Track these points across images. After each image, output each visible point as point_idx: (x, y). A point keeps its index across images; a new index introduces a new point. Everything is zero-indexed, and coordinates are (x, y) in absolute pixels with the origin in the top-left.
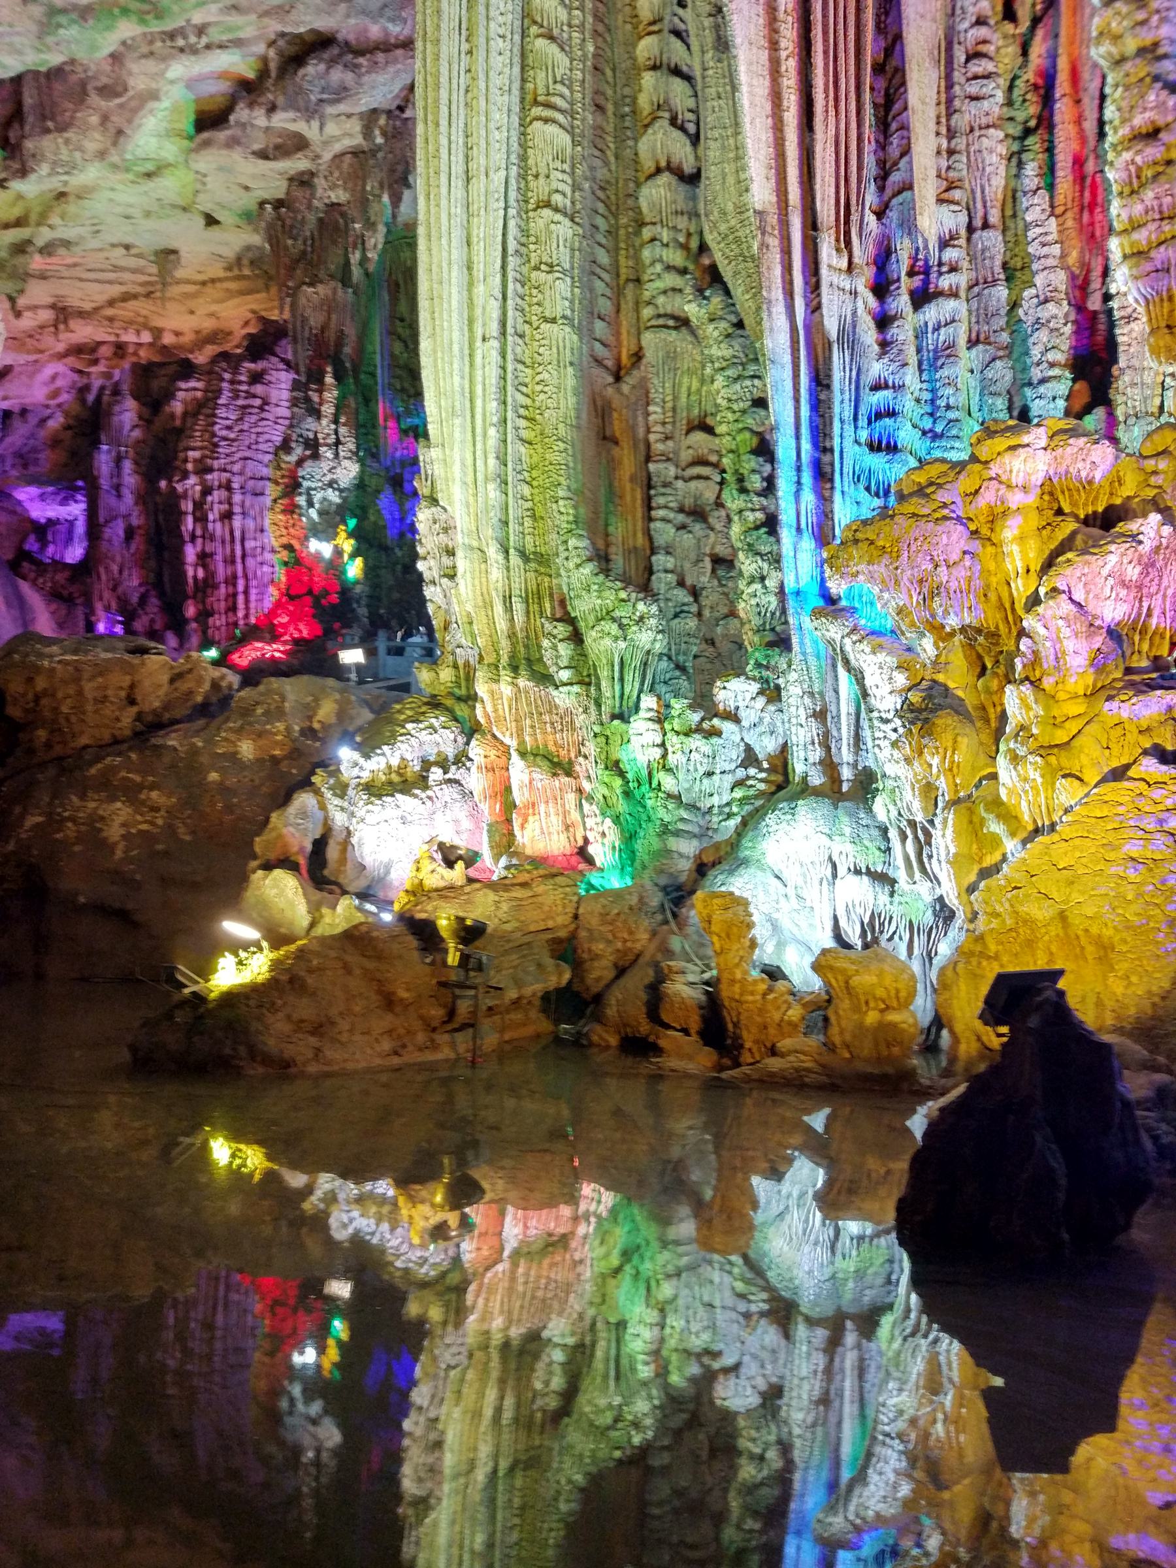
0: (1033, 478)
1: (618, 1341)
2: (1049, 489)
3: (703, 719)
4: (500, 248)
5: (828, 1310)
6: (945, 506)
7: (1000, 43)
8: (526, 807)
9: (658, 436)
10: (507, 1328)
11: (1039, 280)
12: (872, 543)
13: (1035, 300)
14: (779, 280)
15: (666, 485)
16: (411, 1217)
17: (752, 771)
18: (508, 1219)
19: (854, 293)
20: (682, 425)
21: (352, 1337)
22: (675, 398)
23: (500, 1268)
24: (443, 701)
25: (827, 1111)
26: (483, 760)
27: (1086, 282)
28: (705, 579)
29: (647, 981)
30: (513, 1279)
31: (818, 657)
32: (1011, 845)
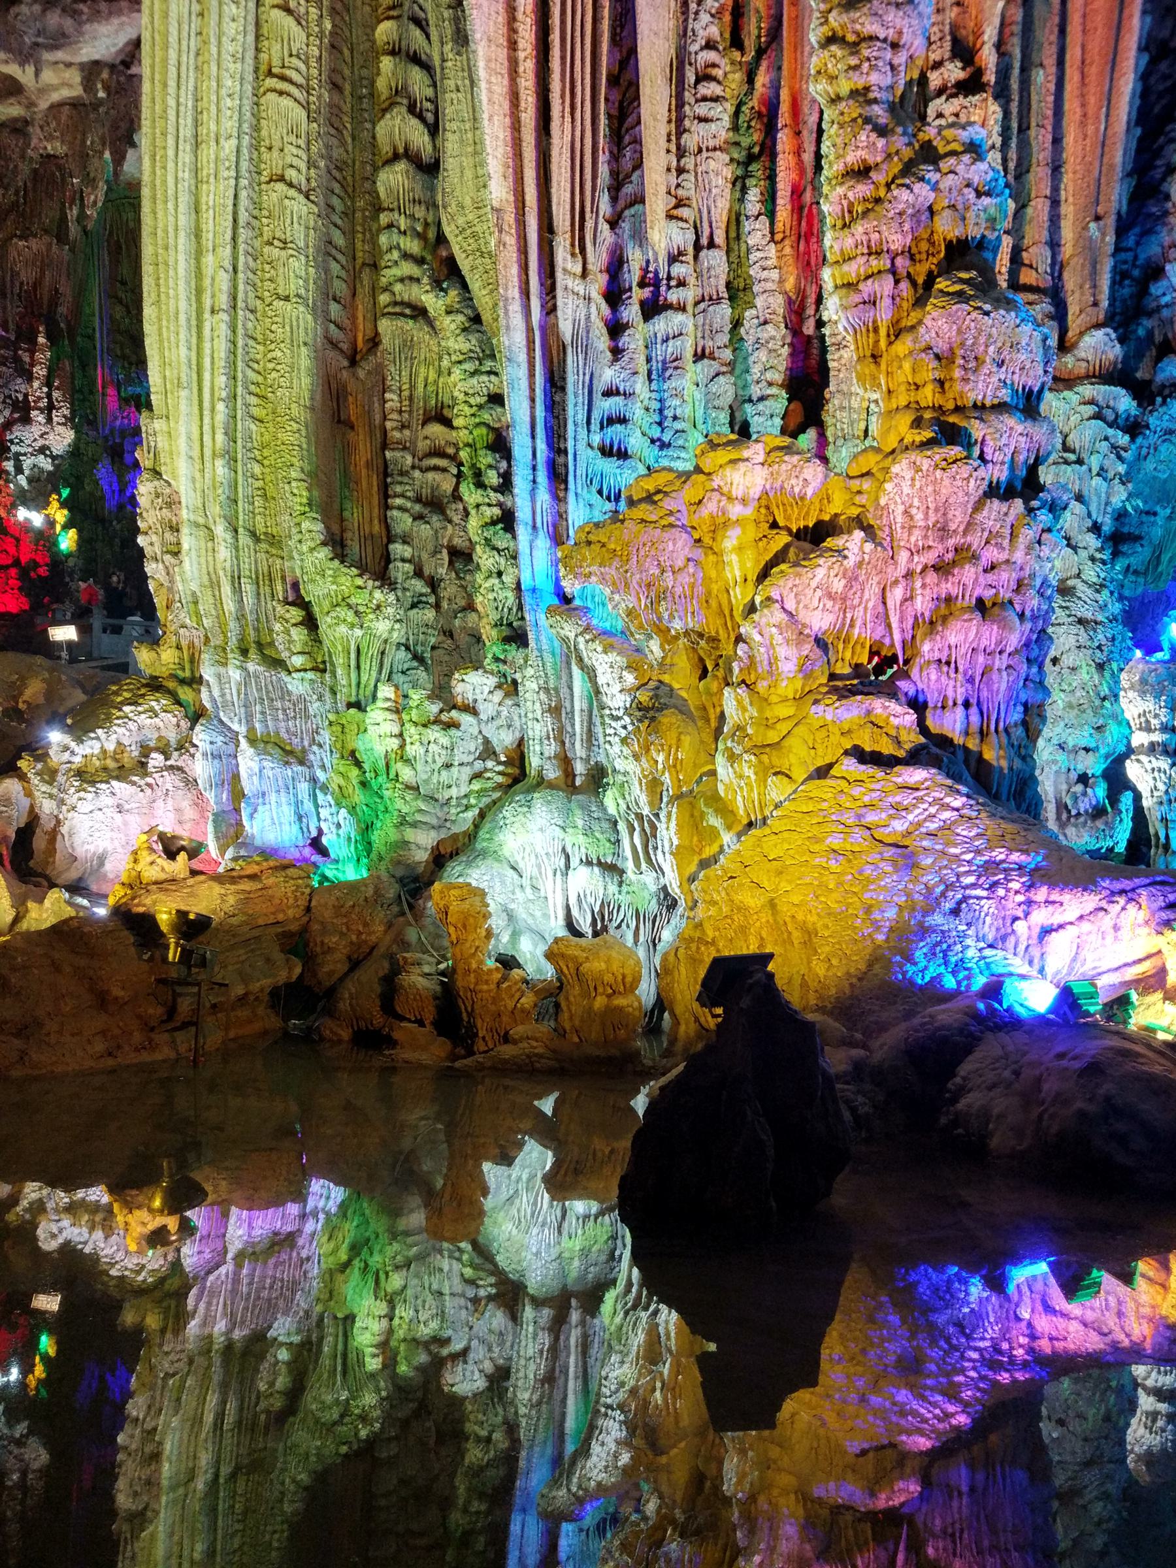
0: (751, 492)
1: (346, 1336)
2: (765, 502)
3: (441, 711)
4: (230, 218)
5: (554, 1286)
6: (671, 513)
7: (728, 68)
8: (256, 796)
9: (395, 424)
10: (230, 1331)
11: (759, 302)
12: (604, 545)
13: (756, 321)
14: (516, 279)
15: (402, 473)
16: (126, 1223)
17: (490, 764)
18: (232, 1220)
19: (588, 299)
20: (419, 415)
21: (58, 1352)
22: (412, 387)
23: (223, 1270)
24: (165, 683)
25: (556, 1095)
26: (208, 747)
27: (802, 307)
28: (442, 571)
29: (381, 974)
30: (236, 1280)
31: (553, 654)
32: (727, 838)
